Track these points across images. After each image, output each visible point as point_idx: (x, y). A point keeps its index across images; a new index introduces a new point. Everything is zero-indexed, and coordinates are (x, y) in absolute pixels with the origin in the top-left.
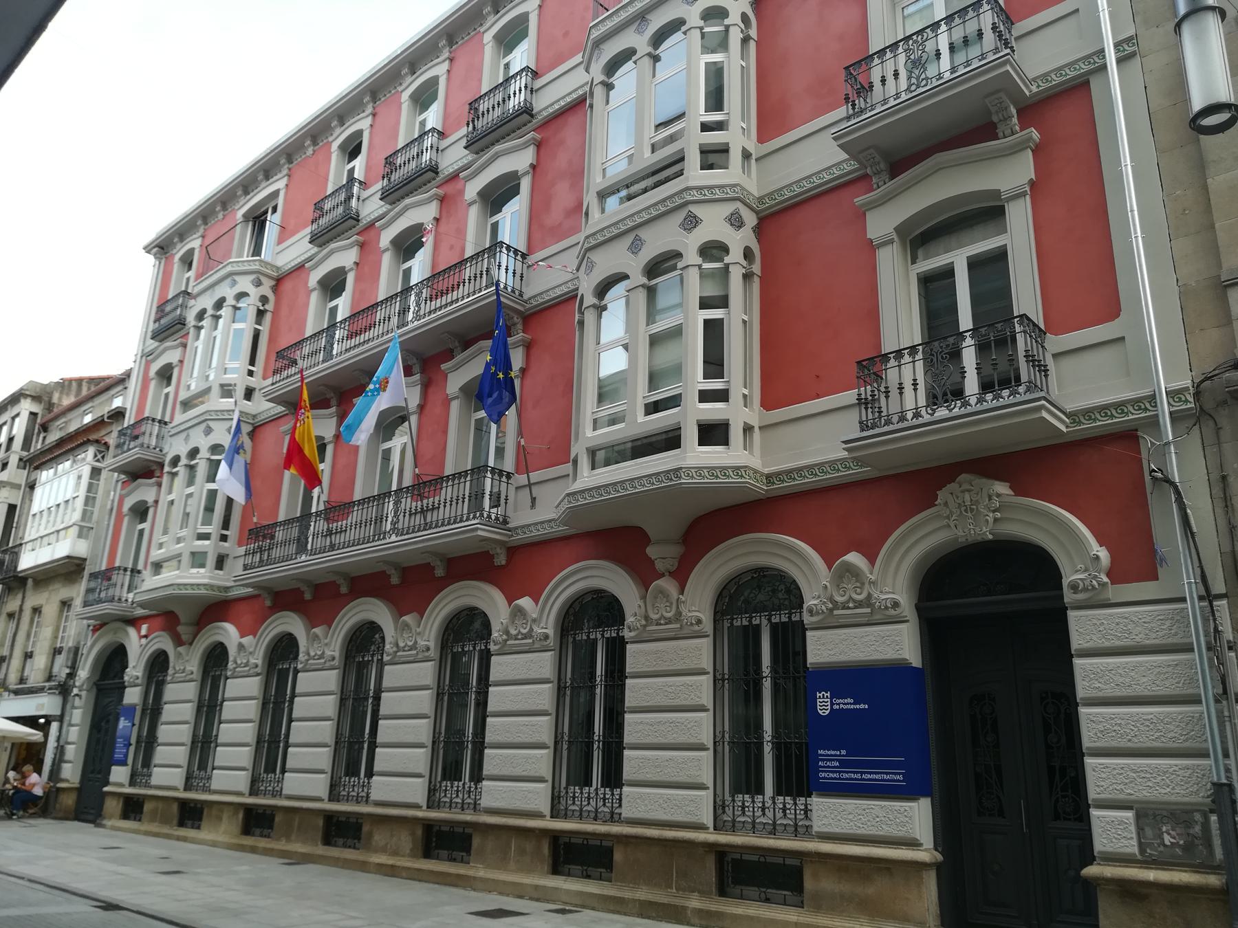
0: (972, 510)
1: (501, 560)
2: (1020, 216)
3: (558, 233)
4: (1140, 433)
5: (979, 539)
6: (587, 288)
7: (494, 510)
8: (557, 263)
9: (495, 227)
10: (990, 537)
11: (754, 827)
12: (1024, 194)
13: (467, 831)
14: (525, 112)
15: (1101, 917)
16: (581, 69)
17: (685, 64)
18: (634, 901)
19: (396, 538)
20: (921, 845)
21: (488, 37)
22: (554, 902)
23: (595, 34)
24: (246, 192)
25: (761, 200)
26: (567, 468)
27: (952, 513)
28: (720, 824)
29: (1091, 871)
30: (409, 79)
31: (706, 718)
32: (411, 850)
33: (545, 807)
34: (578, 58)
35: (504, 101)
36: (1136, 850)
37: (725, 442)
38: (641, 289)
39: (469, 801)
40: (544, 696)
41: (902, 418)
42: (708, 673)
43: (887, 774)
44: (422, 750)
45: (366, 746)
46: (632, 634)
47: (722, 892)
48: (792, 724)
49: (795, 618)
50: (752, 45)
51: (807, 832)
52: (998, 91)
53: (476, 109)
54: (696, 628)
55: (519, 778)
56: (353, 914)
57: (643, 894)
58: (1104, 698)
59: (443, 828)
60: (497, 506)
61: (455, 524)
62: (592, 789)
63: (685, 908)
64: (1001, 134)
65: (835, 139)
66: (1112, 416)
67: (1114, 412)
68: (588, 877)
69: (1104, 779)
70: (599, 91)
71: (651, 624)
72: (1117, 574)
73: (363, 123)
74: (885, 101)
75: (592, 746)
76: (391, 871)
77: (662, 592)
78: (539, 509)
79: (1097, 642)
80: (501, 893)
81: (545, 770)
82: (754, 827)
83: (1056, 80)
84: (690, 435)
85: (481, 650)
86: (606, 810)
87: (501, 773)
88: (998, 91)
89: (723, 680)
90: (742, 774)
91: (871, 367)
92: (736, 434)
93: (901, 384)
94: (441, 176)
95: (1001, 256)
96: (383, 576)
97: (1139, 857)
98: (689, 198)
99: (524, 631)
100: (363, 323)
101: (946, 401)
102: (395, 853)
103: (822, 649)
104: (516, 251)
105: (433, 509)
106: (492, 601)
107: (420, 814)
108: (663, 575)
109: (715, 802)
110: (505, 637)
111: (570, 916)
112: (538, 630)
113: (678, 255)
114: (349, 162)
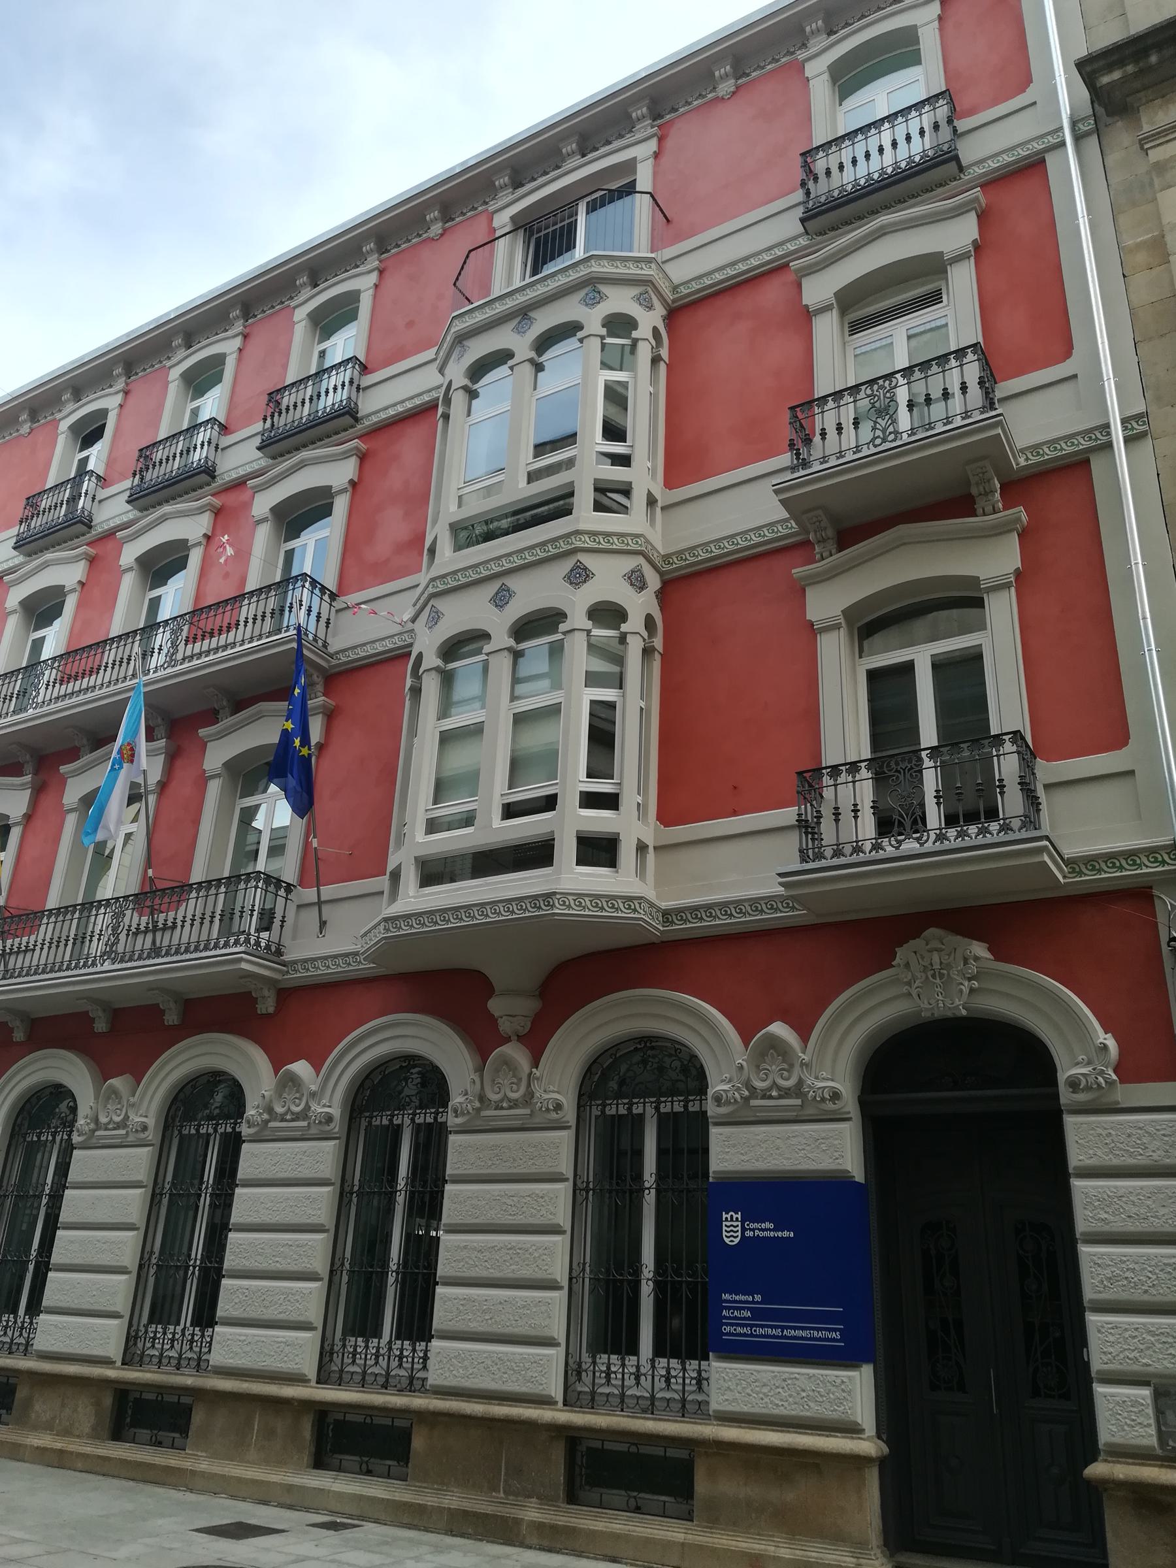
0: (941, 976)
1: (267, 1005)
2: (1002, 612)
3: (381, 572)
4: (1155, 892)
5: (949, 1014)
6: (428, 643)
7: (265, 935)
8: (382, 607)
9: (290, 555)
10: (964, 1012)
11: (622, 1402)
12: (1007, 586)
13: (184, 1400)
14: (347, 413)
15: (1109, 1535)
16: (433, 368)
17: (576, 378)
18: (440, 1510)
19: (106, 966)
20: (862, 1431)
21: (301, 314)
22: (316, 1510)
23: (459, 326)
24: (517, 184)
25: (666, 558)
26: (384, 882)
27: (914, 979)
28: (572, 1397)
29: (1098, 1469)
30: (181, 353)
31: (561, 1243)
32: (94, 1429)
33: (308, 1366)
34: (430, 354)
35: (188, 451)
36: (1154, 1441)
37: (612, 862)
38: (506, 653)
39: (189, 1355)
40: (319, 1204)
41: (858, 850)
42: (566, 1180)
43: (818, 1329)
44: (124, 1277)
45: (31, 1267)
46: (459, 1120)
47: (572, 1498)
48: (676, 1260)
49: (693, 1107)
50: (663, 367)
51: (701, 1411)
52: (984, 458)
53: (278, 403)
54: (554, 1115)
55: (273, 1319)
56: (18, 1534)
57: (453, 1500)
58: (1111, 1233)
59: (146, 1396)
60: (268, 928)
61: (198, 949)
62: (179, 1329)
63: (517, 1522)
64: (980, 511)
65: (776, 492)
66: (1121, 868)
67: (1124, 863)
68: (369, 1472)
69: (1112, 1344)
70: (459, 399)
71: (488, 1107)
72: (1127, 1071)
73: (110, 401)
74: (824, 459)
75: (386, 1275)
76: (59, 1460)
77: (508, 1063)
78: (338, 934)
79: (1102, 1157)
80: (233, 1497)
81: (314, 1312)
82: (622, 1402)
83: (1049, 454)
84: (566, 850)
85: (225, 1135)
86: (402, 1373)
87: (245, 1315)
88: (984, 458)
89: (587, 1190)
90: (608, 1324)
91: (810, 780)
92: (627, 853)
93: (855, 805)
94: (219, 482)
95: (972, 661)
96: (84, 1018)
97: (1159, 1452)
98: (579, 544)
99: (117, 1119)
100: (84, 664)
101: (916, 832)
102: (66, 1433)
103: (732, 1152)
104: (323, 589)
105: (26, 951)
106: (252, 1067)
107: (111, 1373)
108: (507, 1040)
109: (128, 1333)
110: (265, 1116)
111: (347, 1533)
112: (317, 1109)
113: (485, 636)
114: (81, 450)
